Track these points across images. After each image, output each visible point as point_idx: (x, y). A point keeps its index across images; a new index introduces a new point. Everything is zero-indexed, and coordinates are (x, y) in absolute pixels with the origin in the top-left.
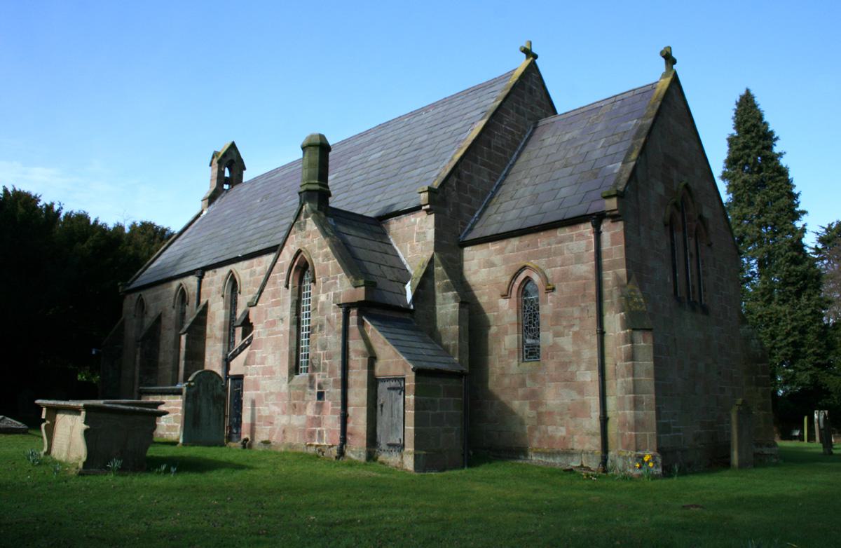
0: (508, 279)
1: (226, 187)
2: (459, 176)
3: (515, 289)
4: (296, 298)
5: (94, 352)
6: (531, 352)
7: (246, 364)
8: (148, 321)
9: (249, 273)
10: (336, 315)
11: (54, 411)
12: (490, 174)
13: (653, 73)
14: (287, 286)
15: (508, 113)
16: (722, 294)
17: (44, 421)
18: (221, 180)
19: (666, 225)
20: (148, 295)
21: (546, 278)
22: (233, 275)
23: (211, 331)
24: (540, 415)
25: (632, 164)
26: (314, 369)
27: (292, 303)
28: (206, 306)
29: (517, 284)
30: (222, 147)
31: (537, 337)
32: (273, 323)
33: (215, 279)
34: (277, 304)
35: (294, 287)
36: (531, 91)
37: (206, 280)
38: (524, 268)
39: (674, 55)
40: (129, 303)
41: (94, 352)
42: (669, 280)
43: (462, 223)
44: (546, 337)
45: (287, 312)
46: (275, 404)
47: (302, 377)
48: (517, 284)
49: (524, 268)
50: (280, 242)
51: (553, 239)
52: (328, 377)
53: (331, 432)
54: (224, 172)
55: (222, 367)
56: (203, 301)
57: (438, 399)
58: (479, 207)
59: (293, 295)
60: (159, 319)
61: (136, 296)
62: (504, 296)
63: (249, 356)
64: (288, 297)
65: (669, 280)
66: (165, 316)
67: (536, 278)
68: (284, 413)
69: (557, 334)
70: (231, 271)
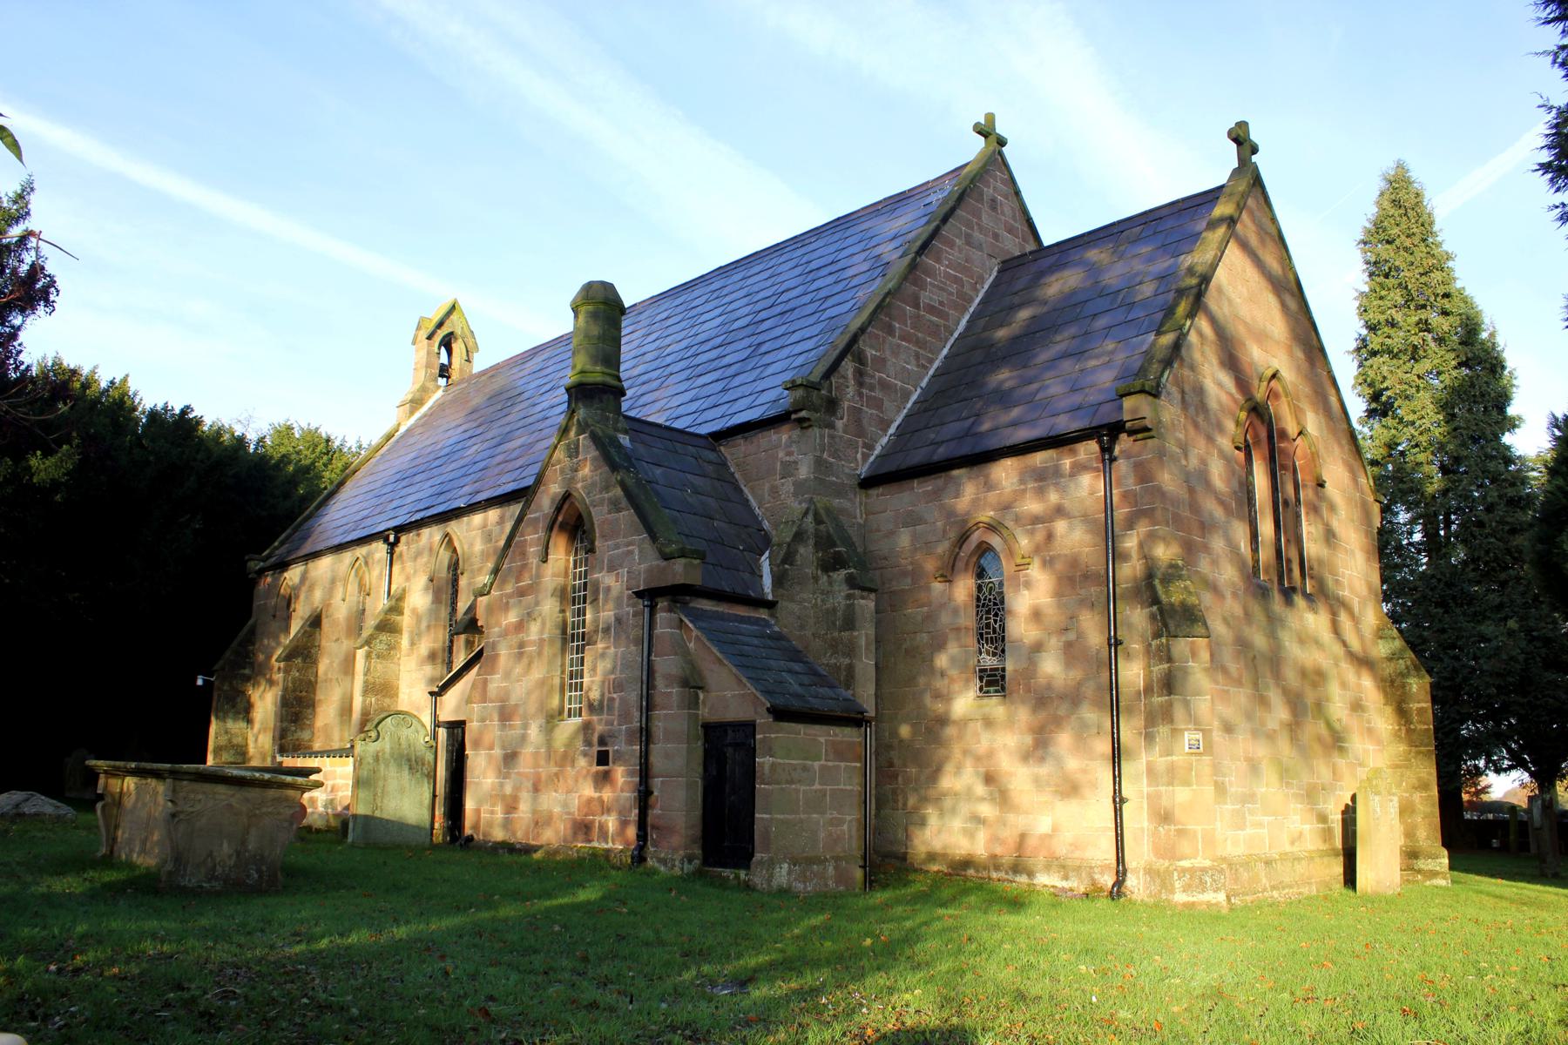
2: (860, 359)
12: (917, 356)
15: (952, 245)
36: (993, 204)
39: (1001, 129)
43: (866, 446)
57: (816, 764)
58: (899, 411)
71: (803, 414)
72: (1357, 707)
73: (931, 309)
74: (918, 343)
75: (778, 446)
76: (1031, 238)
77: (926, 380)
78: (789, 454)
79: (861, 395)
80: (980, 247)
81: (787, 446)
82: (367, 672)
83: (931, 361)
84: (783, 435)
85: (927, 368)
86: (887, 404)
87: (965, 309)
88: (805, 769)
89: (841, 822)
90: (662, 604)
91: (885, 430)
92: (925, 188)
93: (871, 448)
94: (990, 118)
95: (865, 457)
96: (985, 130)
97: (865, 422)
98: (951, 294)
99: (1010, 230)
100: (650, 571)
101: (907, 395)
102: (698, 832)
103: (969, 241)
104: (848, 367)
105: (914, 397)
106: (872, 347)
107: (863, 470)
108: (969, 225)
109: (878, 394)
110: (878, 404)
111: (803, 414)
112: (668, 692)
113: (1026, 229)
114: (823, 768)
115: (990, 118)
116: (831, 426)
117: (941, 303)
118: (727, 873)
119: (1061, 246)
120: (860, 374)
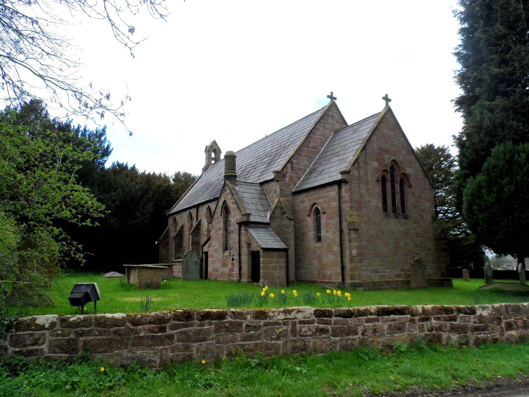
0: (309, 208)
1: (213, 162)
2: (292, 163)
3: (312, 212)
4: (225, 220)
5: (156, 243)
6: (319, 239)
7: (209, 247)
8: (178, 228)
9: (213, 206)
10: (237, 227)
11: (130, 268)
12: (308, 160)
13: (380, 107)
14: (221, 215)
15: (319, 130)
16: (419, 208)
17: (126, 272)
18: (209, 158)
19: (378, 181)
20: (177, 217)
21: (323, 207)
22: (210, 208)
23: (203, 231)
24: (322, 266)
25: (356, 157)
26: (231, 249)
27: (223, 222)
28: (200, 221)
29: (313, 210)
30: (208, 144)
31: (320, 233)
32: (217, 230)
33: (203, 210)
34: (218, 223)
35: (224, 215)
36: (332, 117)
37: (200, 209)
38: (315, 203)
39: (389, 97)
40: (170, 221)
41: (156, 243)
42: (379, 205)
43: (294, 184)
44: (323, 233)
45: (221, 225)
46: (219, 263)
47: (227, 253)
48: (313, 210)
49: (315, 203)
50: (218, 195)
51: (325, 191)
52: (235, 252)
53: (236, 274)
54: (211, 155)
55: (87, 275)
56: (199, 219)
57: (274, 260)
58: (303, 175)
59: (223, 219)
60: (182, 227)
61: (173, 217)
62: (309, 216)
63: (209, 244)
64: (222, 220)
65: (379, 205)
66: (185, 226)
67: (319, 208)
68: (221, 267)
69: (327, 232)
70: (209, 206)
71: (277, 179)
72: (174, 306)
73: (313, 148)
74: (308, 157)
75: (273, 186)
76: (344, 124)
77: (311, 166)
78: (275, 188)
79: (292, 172)
80: (328, 129)
81: (275, 186)
82: (192, 240)
83: (313, 161)
84: (274, 184)
85: (311, 163)
86: (300, 173)
87: (323, 146)
88: (271, 261)
89: (281, 272)
90: (243, 226)
91: (299, 180)
92: (372, 117)
93: (296, 184)
94: (387, 95)
95: (294, 187)
96: (331, 97)
97: (294, 179)
98: (319, 143)
99: (338, 122)
100: (240, 218)
101: (305, 170)
102: (251, 275)
103: (324, 128)
104: (289, 166)
105: (308, 171)
106: (295, 160)
107: (293, 190)
108: (325, 123)
109: (298, 171)
110: (298, 174)
111: (277, 179)
112: (244, 245)
113: (342, 121)
114: (276, 261)
115: (387, 95)
116: (285, 181)
117: (316, 146)
118: (256, 283)
119: (353, 125)
120: (292, 167)
